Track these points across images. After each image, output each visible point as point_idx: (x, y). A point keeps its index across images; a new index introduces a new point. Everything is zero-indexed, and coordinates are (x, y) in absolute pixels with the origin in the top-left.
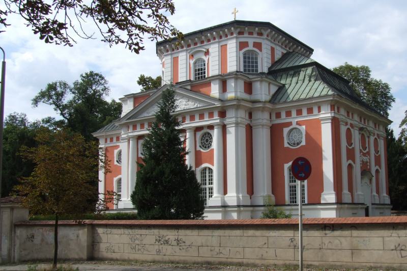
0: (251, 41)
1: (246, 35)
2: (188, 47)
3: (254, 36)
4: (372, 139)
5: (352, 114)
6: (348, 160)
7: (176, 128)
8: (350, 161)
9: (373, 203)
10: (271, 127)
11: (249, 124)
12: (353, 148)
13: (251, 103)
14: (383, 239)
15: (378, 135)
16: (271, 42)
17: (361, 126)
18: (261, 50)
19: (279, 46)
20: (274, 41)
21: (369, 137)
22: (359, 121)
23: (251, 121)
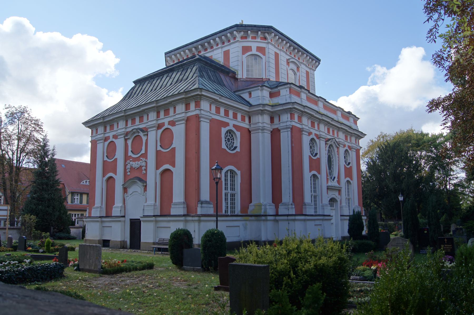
0: (254, 45)
1: (250, 39)
2: (205, 51)
3: (256, 40)
4: (342, 150)
5: (318, 125)
6: (345, 178)
7: (372, 164)
8: (348, 179)
9: (342, 214)
10: (271, 132)
11: (248, 129)
12: (351, 167)
13: (271, 107)
14: (277, 211)
15: (349, 147)
16: (275, 47)
17: (329, 137)
18: (264, 54)
19: (284, 51)
20: (278, 46)
21: (338, 148)
22: (326, 132)
23: (250, 125)
